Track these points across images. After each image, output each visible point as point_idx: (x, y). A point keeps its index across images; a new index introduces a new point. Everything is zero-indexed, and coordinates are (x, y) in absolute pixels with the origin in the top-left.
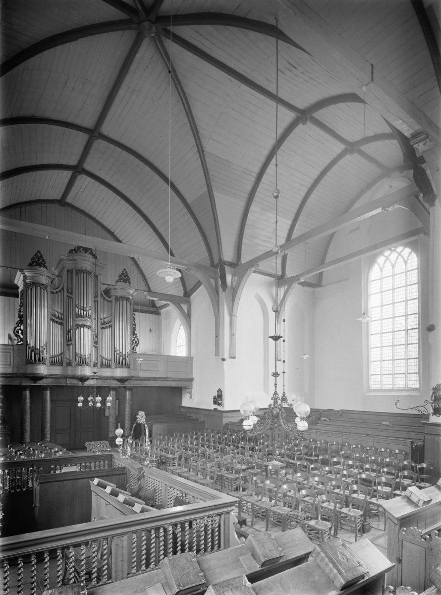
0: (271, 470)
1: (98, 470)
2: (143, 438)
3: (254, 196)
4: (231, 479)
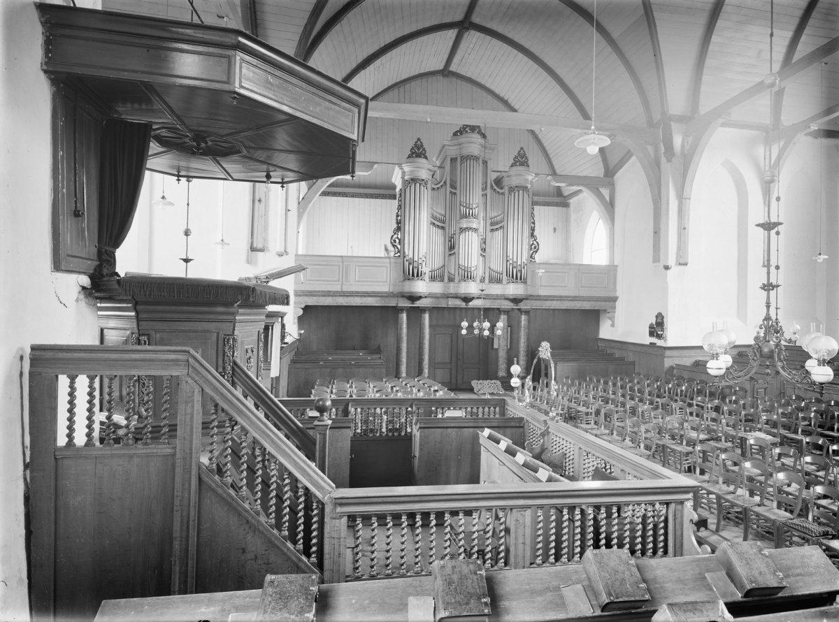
0: (751, 445)
1: (487, 419)
2: (543, 382)
4: (680, 452)
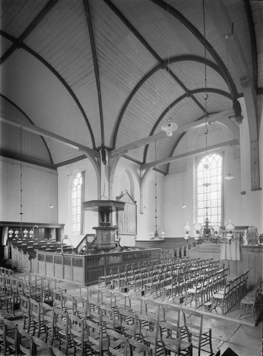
3: (120, 122)
